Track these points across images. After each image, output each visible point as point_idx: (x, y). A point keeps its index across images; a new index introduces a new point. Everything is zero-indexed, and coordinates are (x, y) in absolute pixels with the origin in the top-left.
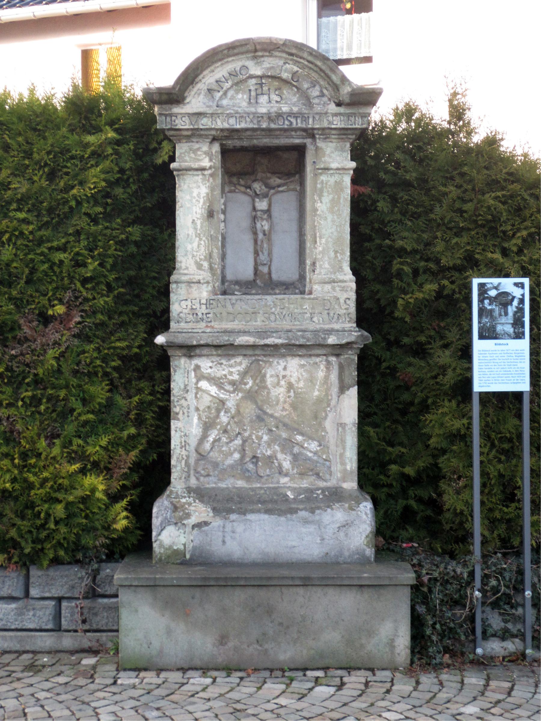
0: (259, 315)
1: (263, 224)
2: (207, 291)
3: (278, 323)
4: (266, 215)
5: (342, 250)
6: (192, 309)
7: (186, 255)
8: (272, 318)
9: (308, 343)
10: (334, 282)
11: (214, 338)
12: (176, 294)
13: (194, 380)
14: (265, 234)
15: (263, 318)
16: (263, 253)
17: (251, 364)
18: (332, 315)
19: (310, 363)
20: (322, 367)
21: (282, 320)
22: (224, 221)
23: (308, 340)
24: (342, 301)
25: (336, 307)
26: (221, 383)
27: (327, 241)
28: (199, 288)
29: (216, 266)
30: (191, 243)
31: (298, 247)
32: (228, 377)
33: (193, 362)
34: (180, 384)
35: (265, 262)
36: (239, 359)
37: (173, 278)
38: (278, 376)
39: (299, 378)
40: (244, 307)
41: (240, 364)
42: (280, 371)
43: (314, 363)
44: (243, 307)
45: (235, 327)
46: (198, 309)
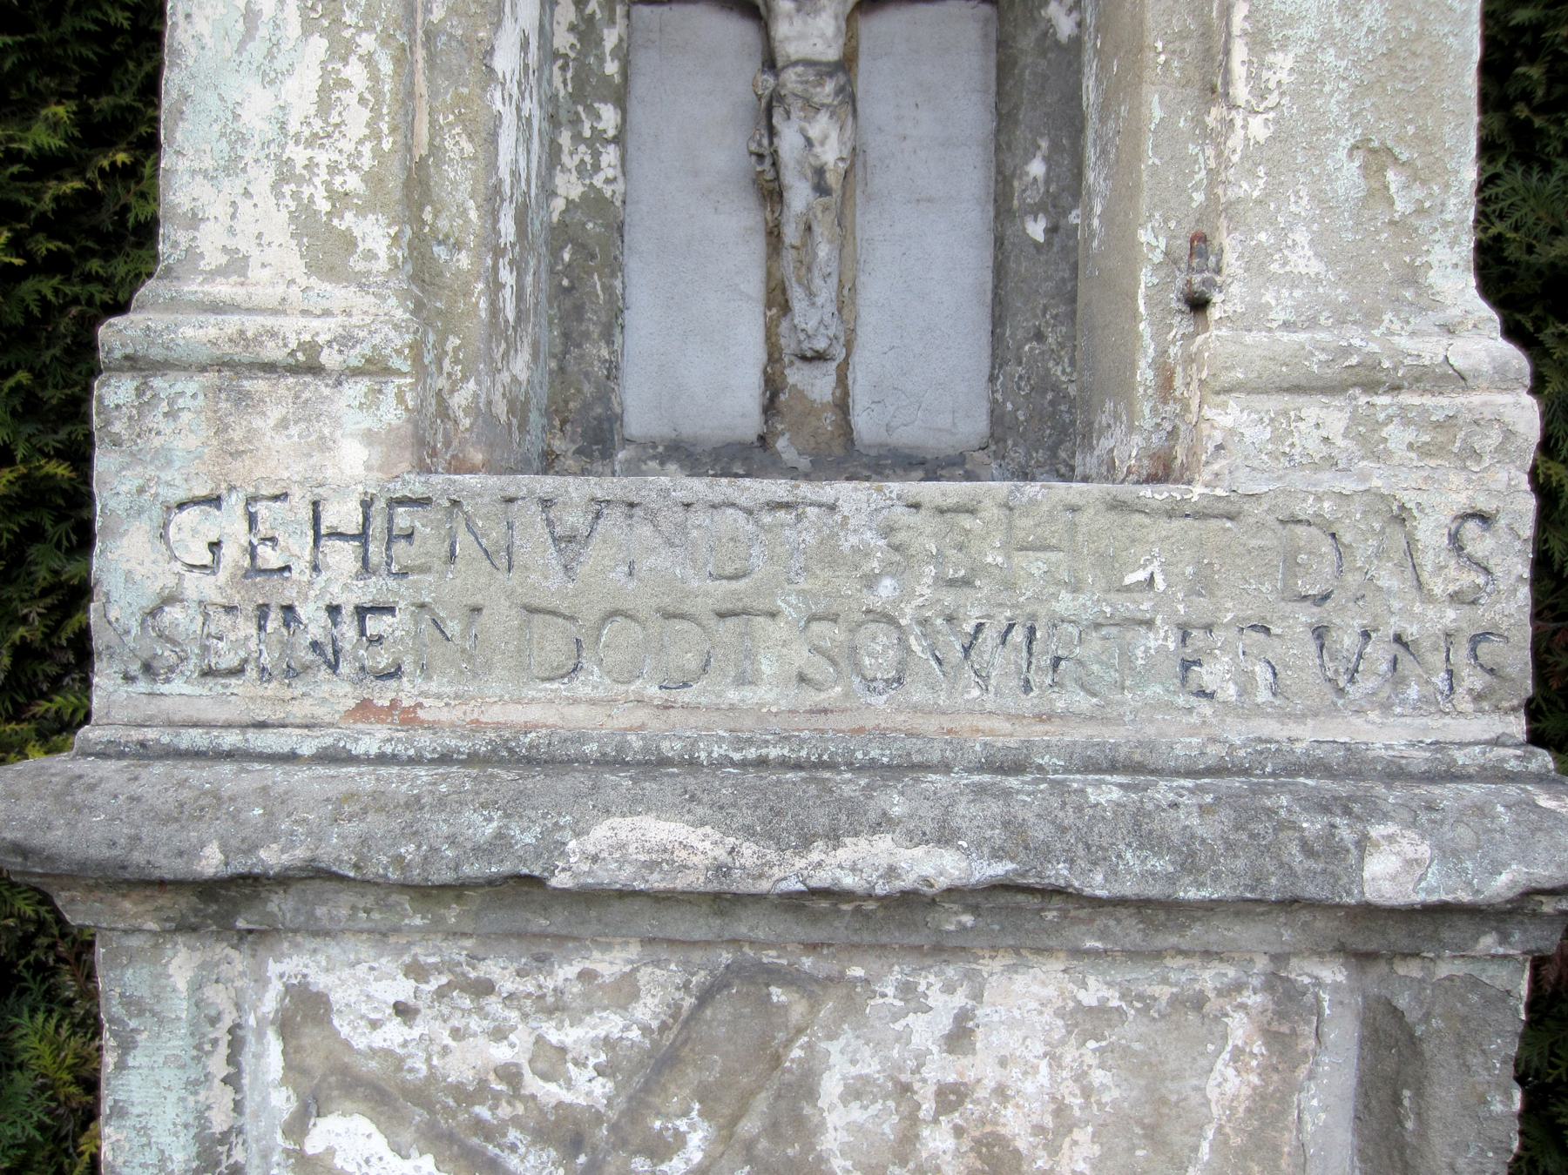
0: (777, 630)
1: (814, 132)
2: (369, 437)
3: (918, 694)
4: (829, 87)
5: (1426, 140)
6: (255, 571)
7: (232, 166)
8: (879, 652)
9: (1190, 893)
10: (1371, 387)
11: (376, 823)
12: (135, 458)
13: (282, 1102)
14: (821, 189)
15: (800, 656)
16: (811, 295)
17: (706, 997)
18: (1348, 641)
19: (1147, 1002)
20: (1239, 1028)
21: (952, 677)
22: (618, 140)
23: (1189, 864)
24: (1430, 533)
25: (1387, 578)
26: (479, 1125)
27: (1308, 72)
28: (307, 413)
29: (464, 260)
30: (269, 80)
31: (988, 277)
32: (533, 1084)
33: (273, 968)
34: (162, 1137)
35: (821, 344)
36: (610, 964)
37: (114, 335)
38: (906, 1089)
39: (1060, 1110)
40: (659, 560)
41: (625, 992)
42: (921, 1058)
43: (1174, 1001)
44: (646, 563)
45: (579, 715)
46: (301, 571)
